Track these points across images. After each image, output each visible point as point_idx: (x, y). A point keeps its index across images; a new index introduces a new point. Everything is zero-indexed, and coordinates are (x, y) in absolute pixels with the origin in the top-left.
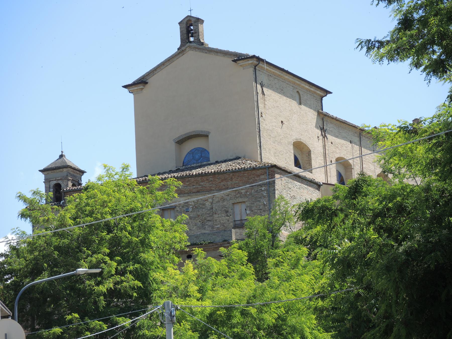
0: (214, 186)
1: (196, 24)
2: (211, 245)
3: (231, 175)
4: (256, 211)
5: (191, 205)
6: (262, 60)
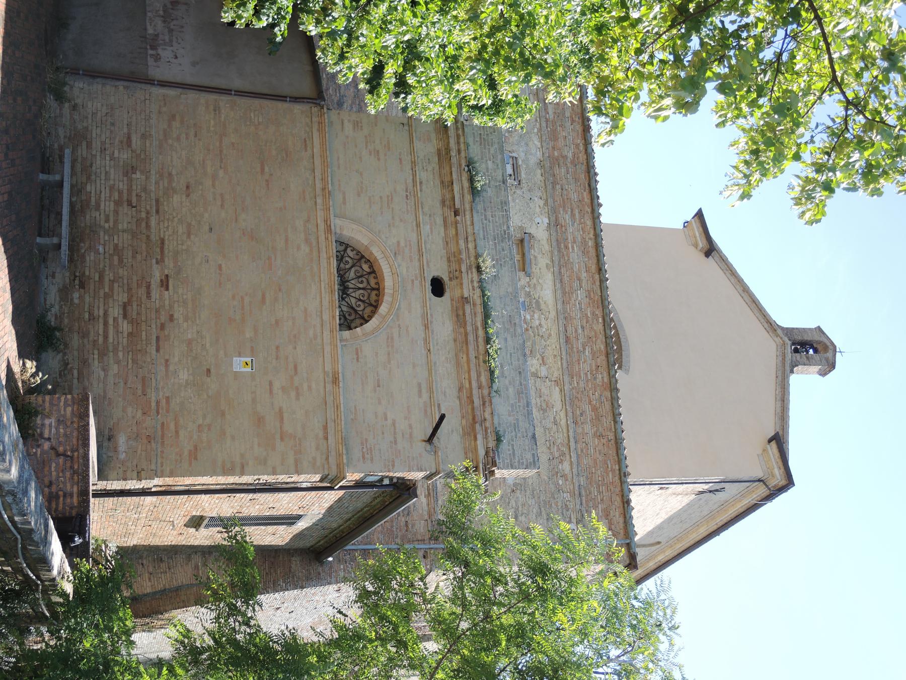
0: (582, 385)
1: (824, 361)
2: (484, 379)
3: (611, 436)
4: (513, 503)
5: (532, 317)
6: (770, 497)
